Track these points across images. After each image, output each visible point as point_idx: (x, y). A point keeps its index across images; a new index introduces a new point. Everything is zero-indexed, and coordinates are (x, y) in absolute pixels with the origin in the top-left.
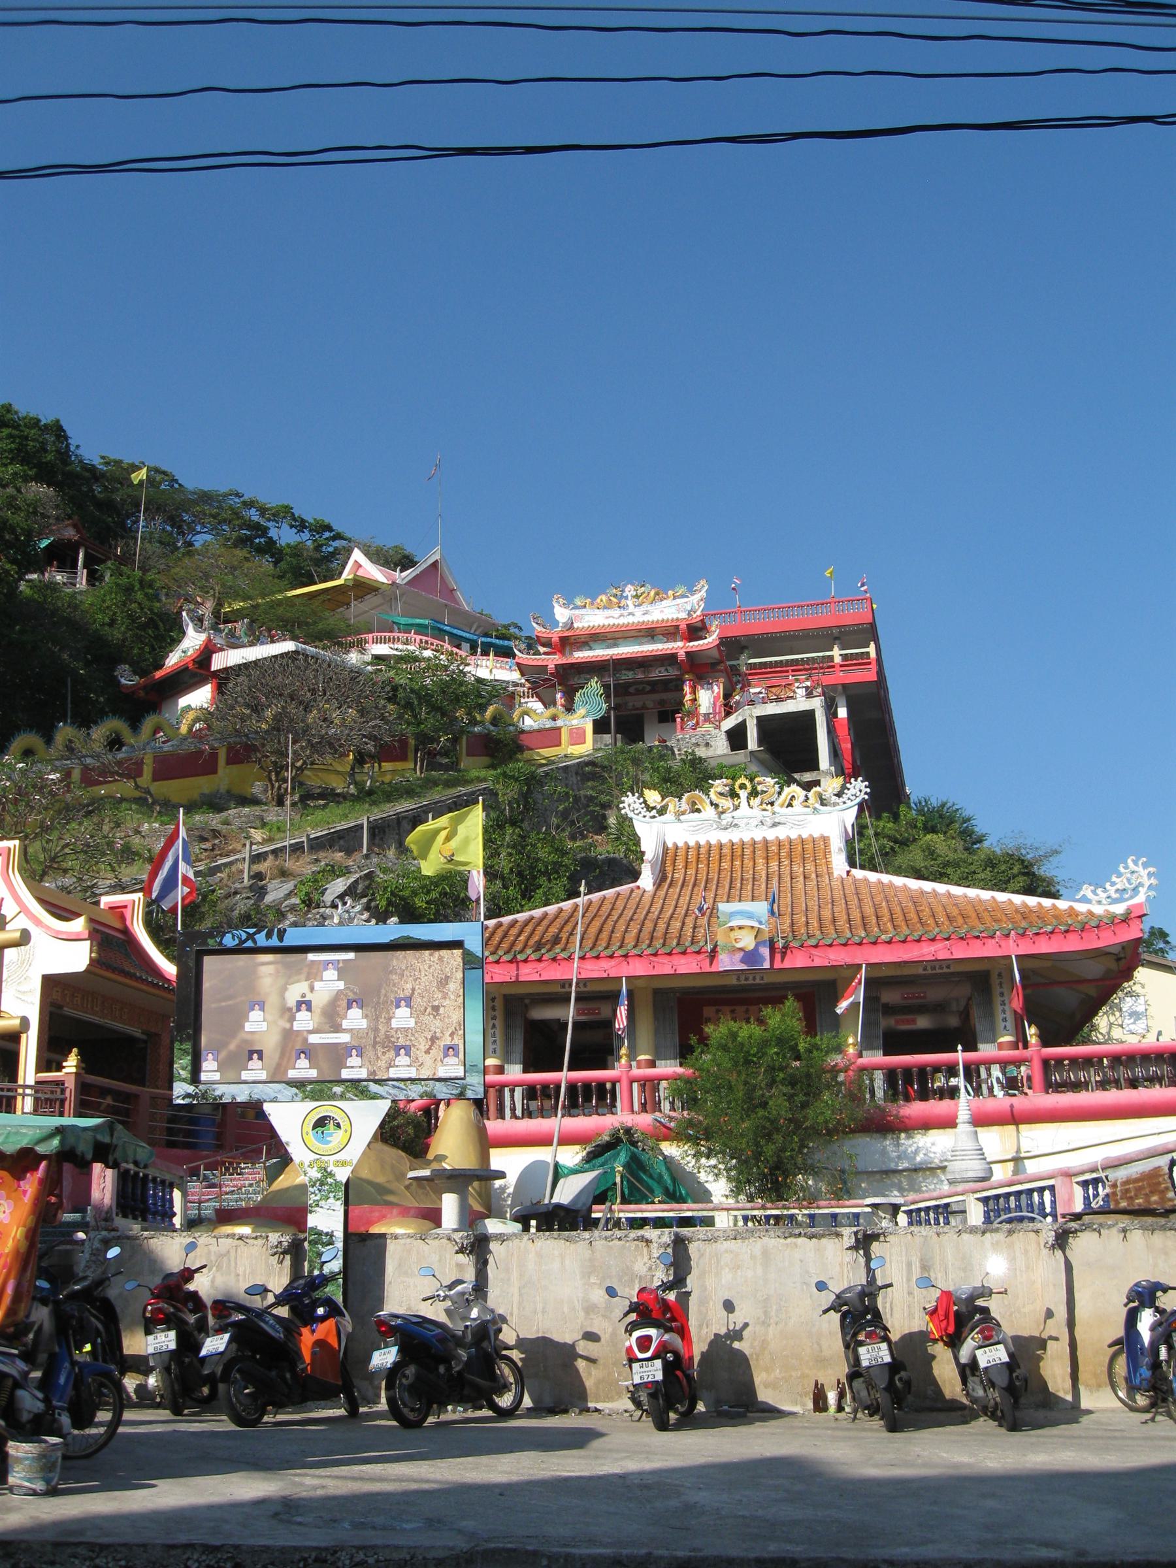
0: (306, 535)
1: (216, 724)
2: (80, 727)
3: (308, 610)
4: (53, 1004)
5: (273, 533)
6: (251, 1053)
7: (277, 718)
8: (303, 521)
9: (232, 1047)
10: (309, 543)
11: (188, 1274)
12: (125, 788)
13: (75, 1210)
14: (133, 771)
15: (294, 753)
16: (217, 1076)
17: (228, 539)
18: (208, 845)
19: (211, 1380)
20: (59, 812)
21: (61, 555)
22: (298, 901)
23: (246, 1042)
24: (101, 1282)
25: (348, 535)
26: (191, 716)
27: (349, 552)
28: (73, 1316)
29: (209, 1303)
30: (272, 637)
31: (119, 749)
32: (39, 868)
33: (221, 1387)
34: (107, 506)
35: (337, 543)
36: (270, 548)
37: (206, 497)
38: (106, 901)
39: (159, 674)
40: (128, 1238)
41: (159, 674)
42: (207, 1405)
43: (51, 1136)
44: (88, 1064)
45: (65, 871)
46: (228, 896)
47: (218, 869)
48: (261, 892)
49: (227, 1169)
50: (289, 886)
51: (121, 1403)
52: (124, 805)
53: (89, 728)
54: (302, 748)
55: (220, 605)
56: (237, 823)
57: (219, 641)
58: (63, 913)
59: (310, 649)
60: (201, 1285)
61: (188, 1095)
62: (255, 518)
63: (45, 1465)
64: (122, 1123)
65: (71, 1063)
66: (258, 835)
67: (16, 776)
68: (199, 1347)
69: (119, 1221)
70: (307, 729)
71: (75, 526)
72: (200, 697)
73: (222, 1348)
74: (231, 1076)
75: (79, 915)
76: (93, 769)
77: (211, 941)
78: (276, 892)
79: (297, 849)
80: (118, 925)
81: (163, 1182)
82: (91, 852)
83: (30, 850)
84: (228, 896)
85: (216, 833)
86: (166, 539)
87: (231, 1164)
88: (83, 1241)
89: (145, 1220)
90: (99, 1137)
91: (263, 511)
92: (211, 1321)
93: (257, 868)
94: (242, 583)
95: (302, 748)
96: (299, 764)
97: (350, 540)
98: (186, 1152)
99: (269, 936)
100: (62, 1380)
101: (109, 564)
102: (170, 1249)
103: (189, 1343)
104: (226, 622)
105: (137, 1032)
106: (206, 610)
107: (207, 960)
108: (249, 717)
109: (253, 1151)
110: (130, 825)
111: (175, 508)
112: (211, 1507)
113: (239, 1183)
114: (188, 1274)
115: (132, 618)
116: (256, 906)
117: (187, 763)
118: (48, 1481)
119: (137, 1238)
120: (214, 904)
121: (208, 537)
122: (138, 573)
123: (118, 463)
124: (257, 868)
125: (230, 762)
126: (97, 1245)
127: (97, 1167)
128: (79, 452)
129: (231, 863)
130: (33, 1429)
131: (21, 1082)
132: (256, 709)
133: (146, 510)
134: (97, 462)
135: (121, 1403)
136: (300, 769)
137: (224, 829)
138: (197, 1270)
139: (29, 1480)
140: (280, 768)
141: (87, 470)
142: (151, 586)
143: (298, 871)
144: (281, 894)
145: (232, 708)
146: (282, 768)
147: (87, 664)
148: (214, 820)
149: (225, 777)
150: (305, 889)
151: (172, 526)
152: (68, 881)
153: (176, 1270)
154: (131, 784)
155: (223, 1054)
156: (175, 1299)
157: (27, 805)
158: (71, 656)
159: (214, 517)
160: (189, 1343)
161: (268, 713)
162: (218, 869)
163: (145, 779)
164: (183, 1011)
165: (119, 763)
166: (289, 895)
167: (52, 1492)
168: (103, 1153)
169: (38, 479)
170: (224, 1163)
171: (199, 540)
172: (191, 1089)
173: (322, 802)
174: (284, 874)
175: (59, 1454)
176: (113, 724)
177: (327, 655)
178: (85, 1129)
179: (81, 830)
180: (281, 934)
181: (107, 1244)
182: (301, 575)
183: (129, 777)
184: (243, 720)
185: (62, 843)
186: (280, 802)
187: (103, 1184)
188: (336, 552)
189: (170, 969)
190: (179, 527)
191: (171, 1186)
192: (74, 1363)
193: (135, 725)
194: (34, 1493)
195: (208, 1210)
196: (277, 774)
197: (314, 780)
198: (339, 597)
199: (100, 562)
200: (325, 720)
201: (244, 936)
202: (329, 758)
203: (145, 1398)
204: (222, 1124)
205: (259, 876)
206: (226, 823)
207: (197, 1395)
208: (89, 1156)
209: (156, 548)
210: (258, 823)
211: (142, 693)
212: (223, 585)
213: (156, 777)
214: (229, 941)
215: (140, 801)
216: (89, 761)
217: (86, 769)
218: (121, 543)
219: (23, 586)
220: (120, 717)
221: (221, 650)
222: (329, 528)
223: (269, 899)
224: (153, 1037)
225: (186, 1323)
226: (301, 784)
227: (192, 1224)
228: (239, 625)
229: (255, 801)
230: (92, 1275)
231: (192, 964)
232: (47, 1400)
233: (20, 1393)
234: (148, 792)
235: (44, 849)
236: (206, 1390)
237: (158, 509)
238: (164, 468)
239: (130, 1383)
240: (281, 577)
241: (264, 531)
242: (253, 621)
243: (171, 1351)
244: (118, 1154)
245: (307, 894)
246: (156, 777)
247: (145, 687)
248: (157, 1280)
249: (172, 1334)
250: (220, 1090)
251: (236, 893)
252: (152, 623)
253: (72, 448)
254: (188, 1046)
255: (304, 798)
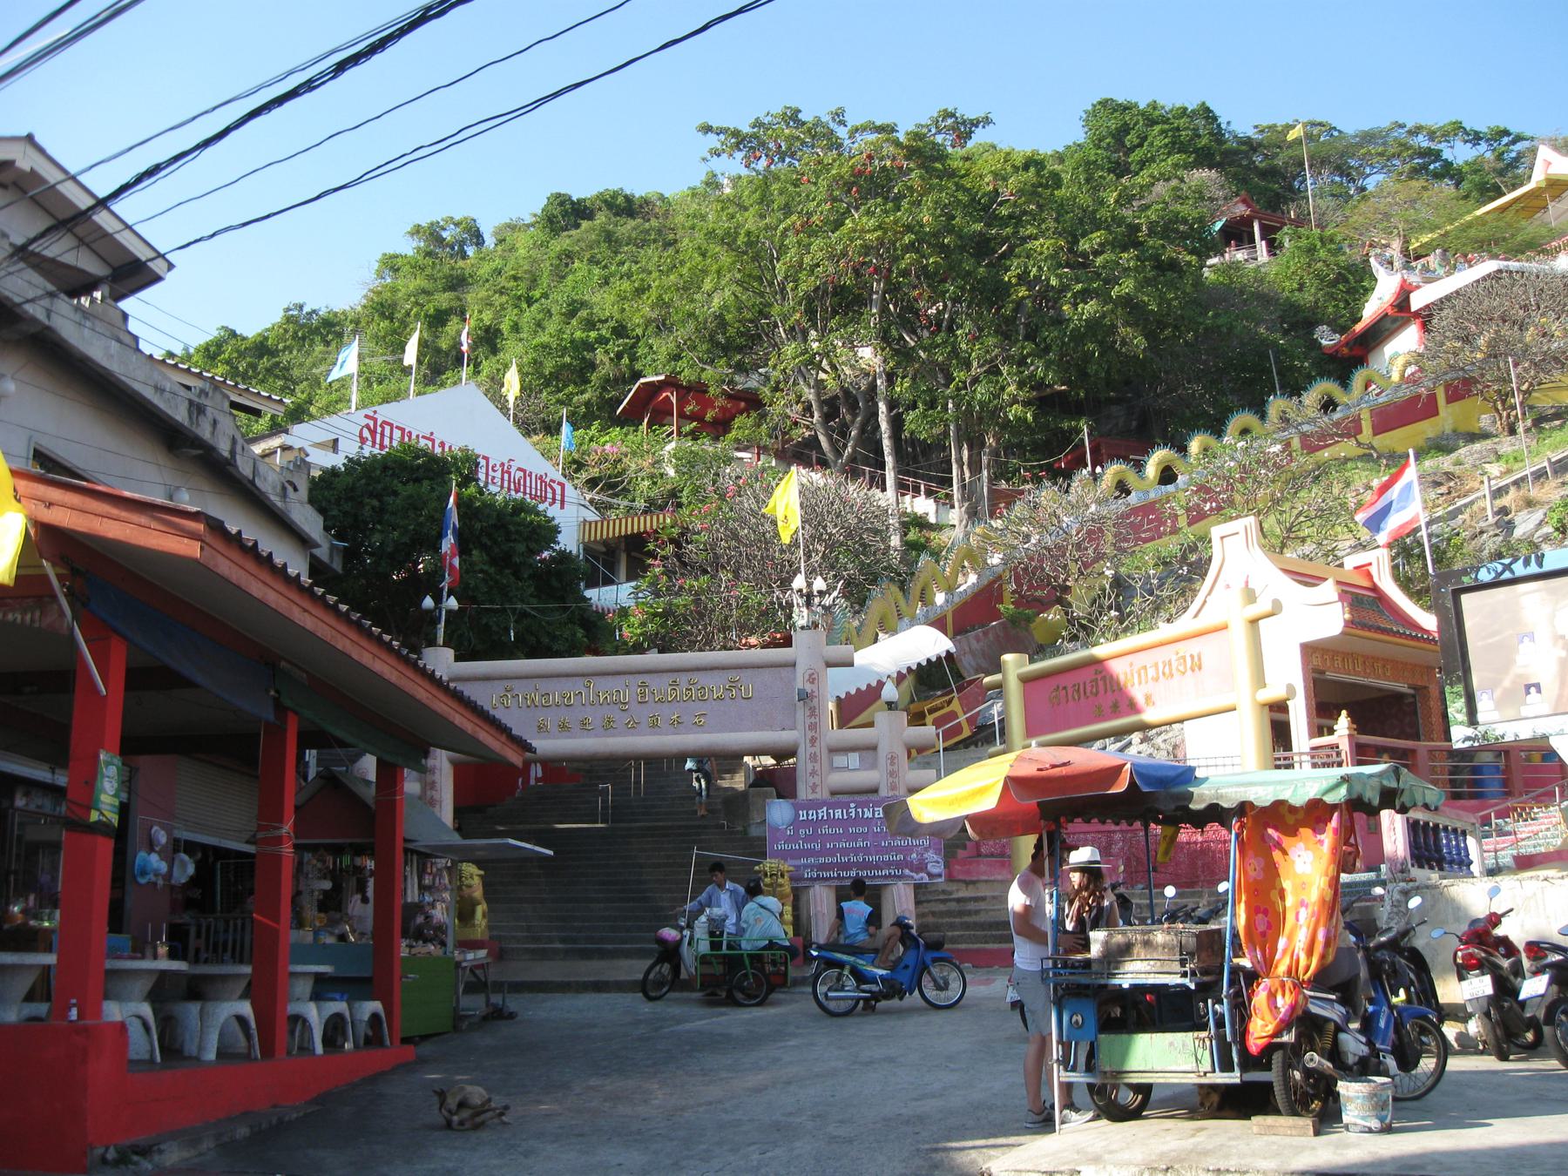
0: (1483, 147)
1: (1428, 364)
2: (1291, 396)
3: (1502, 224)
4: (1314, 670)
5: (1447, 155)
6: (1528, 687)
7: (1492, 344)
8: (1476, 133)
9: (1507, 683)
10: (1488, 155)
11: (1495, 919)
12: (1346, 448)
13: (1369, 870)
14: (1352, 429)
15: (1518, 377)
16: (1495, 716)
17: (1401, 174)
18: (1443, 489)
19: (1533, 1024)
20: (1287, 482)
21: (1237, 234)
22: (1551, 530)
23: (1519, 676)
24: (1405, 933)
25: (1528, 134)
26: (1400, 361)
27: (1533, 151)
28: (1384, 961)
29: (1521, 947)
30: (1469, 262)
31: (1334, 410)
32: (1277, 542)
33: (1546, 1029)
34: (1271, 173)
35: (1519, 146)
36: (1448, 171)
37: (1369, 137)
38: (1351, 562)
39: (1359, 327)
40: (1427, 887)
41: (1359, 327)
42: (1533, 1049)
43: (1337, 786)
44: (1361, 724)
45: (1303, 540)
46: (1474, 537)
47: (1459, 511)
48: (1509, 526)
49: (1520, 815)
50: (1538, 515)
51: (1445, 1051)
52: (1349, 465)
53: (1300, 395)
54: (1525, 370)
55: (1407, 242)
56: (1469, 462)
57: (1414, 279)
58: (1309, 580)
59: (1513, 265)
60: (1515, 930)
61: (1468, 739)
62: (1425, 144)
63: (1377, 1104)
64: (1405, 766)
65: (1343, 723)
66: (1494, 469)
67: (1238, 455)
68: (1516, 992)
69: (1416, 872)
70: (1526, 348)
71: (1244, 201)
72: (1407, 341)
73: (1542, 991)
74: (1511, 713)
75: (1325, 579)
76: (1312, 435)
77: (1465, 579)
78: (1525, 523)
79: (1540, 475)
80: (1365, 583)
81: (1455, 830)
82: (1325, 515)
83: (1265, 526)
84: (1474, 537)
85: (1449, 476)
86: (1337, 191)
87: (1523, 809)
88: (1381, 898)
89: (1441, 869)
90: (1385, 783)
91: (1432, 135)
92: (1526, 963)
93: (1499, 503)
94: (1425, 214)
95: (1525, 370)
96: (1525, 387)
97: (1532, 139)
98: (1473, 802)
99: (1527, 563)
100: (1382, 1024)
101: (1285, 229)
102: (1473, 895)
103: (1505, 988)
104: (1417, 258)
105: (1402, 687)
106: (1395, 250)
107: (1464, 598)
108: (1462, 349)
109: (1545, 794)
110: (1358, 484)
111: (1341, 158)
112: (1552, 1145)
113: (1535, 828)
114: (1495, 919)
115: (1320, 277)
116: (1506, 542)
117: (1407, 411)
118: (1382, 1120)
119: (1436, 887)
120: (1459, 547)
121: (1380, 177)
122: (1316, 231)
123: (1272, 128)
124: (1499, 503)
125: (1450, 399)
126: (1397, 896)
127: (1386, 815)
128: (1231, 128)
129: (1472, 503)
130: (1363, 1069)
131: (1295, 749)
132: (1467, 339)
133: (1311, 166)
134: (1251, 133)
135: (1445, 1051)
136: (1528, 392)
137: (1457, 470)
138: (1503, 915)
139: (1363, 1118)
140: (1505, 396)
141: (1244, 143)
142: (1332, 241)
143: (1544, 498)
144: (1531, 525)
145: (1442, 344)
146: (1507, 395)
147: (1286, 333)
148: (1446, 463)
149: (1448, 416)
150: (1556, 516)
151: (1341, 176)
152: (1308, 548)
153: (1482, 916)
154: (1353, 442)
155: (1498, 693)
156: (1484, 944)
157: (1255, 480)
158: (1267, 329)
159: (1381, 154)
160: (1505, 988)
161: (1481, 342)
162: (1459, 511)
163: (1366, 433)
164: (1453, 654)
165: (1337, 424)
166: (1540, 524)
167: (1387, 1130)
168: (1389, 798)
169: (1198, 164)
170: (1515, 809)
171: (1371, 183)
172: (1470, 732)
173: (1557, 422)
174: (1530, 504)
175: (1390, 1093)
176: (1323, 387)
177: (1533, 266)
178: (1371, 776)
179: (1312, 496)
180: (1540, 561)
181: (1407, 895)
182: (1488, 190)
183: (1349, 436)
184: (1455, 354)
185: (1295, 512)
186: (1512, 431)
187: (1393, 832)
188: (1520, 156)
189: (1428, 621)
190: (1348, 175)
191: (1464, 833)
192: (1391, 1007)
193: (1344, 382)
194: (1370, 1131)
195: (1506, 858)
196: (1504, 402)
197: (1545, 401)
198: (1534, 203)
199: (1277, 230)
200: (1544, 335)
201: (1500, 568)
202: (1557, 375)
203: (1468, 1046)
204: (1507, 770)
205: (1504, 511)
206: (1459, 463)
207: (1521, 1041)
208: (1376, 802)
209: (1331, 202)
210: (1493, 458)
211: (1346, 350)
212: (1406, 221)
213: (1377, 430)
214: (1485, 576)
215: (1366, 458)
216: (1306, 428)
217: (1304, 437)
218: (1292, 206)
219: (1206, 272)
220: (1329, 377)
221: (1418, 287)
222: (1506, 133)
223: (1518, 533)
224: (1421, 690)
225: (1499, 967)
226: (1531, 408)
227: (1492, 872)
228: (1431, 259)
229: (1485, 436)
230: (1397, 926)
231: (1450, 604)
232: (1370, 1043)
233: (1342, 1036)
234: (1372, 448)
235: (1279, 522)
236: (1530, 1036)
237: (1322, 163)
238: (1319, 120)
239: (1450, 1030)
240: (1466, 197)
241: (1437, 155)
242: (1445, 251)
243: (1489, 997)
244: (1405, 798)
245: (1560, 520)
246: (1377, 430)
247: (1347, 344)
248: (1464, 928)
249: (1487, 979)
250: (1499, 730)
251: (1482, 532)
252: (1341, 278)
253: (1223, 126)
254: (1459, 688)
255: (1538, 422)
